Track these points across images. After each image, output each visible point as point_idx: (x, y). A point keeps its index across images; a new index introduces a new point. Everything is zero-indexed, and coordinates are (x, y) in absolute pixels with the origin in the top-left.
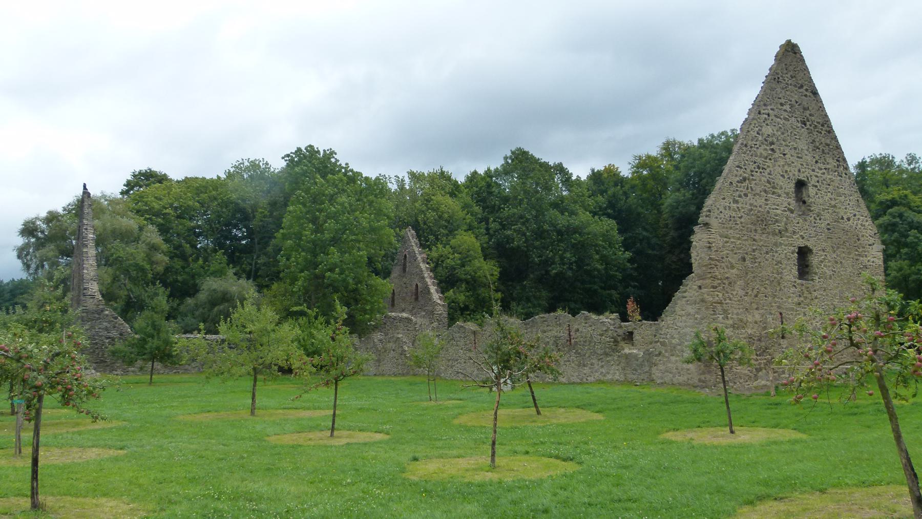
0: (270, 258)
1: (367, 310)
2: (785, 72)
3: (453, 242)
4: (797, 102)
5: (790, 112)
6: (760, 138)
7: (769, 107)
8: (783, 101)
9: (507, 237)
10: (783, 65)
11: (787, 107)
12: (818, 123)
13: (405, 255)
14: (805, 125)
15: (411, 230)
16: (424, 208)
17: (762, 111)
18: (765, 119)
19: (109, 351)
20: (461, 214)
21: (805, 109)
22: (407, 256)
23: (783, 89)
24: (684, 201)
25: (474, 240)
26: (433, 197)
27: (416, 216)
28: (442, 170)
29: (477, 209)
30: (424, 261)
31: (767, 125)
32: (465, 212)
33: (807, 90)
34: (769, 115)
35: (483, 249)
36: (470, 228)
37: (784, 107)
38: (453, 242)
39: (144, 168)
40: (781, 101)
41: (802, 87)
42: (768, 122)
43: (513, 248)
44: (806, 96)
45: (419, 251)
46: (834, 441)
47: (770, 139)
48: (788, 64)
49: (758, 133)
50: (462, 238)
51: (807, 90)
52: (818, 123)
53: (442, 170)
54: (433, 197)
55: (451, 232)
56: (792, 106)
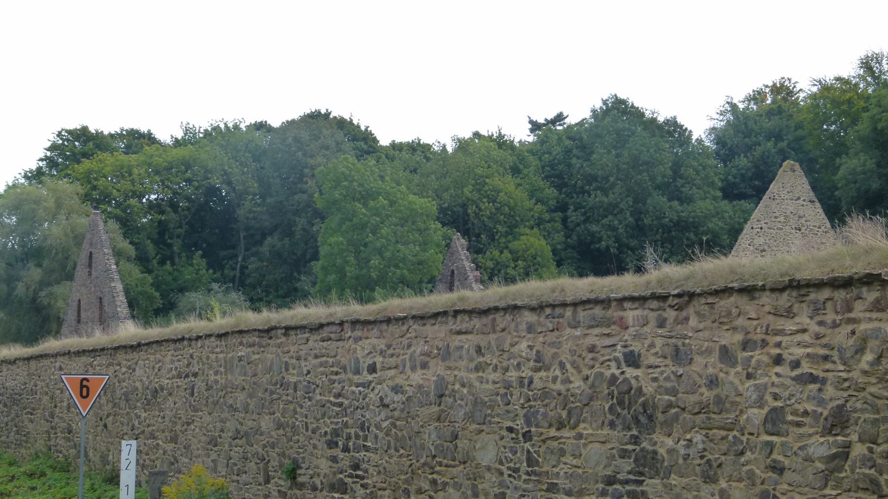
0: (262, 261)
1: (179, 206)
2: (782, 189)
3: (515, 245)
4: (792, 213)
5: (784, 222)
6: (752, 248)
7: (762, 222)
8: (777, 214)
9: (592, 235)
10: (780, 184)
11: (782, 219)
12: (814, 226)
13: (453, 272)
14: (800, 230)
15: (460, 237)
16: (476, 196)
17: (755, 227)
18: (758, 232)
19: (560, 414)
20: (528, 204)
21: (800, 217)
22: (456, 272)
23: (778, 204)
24: (864, 173)
25: (543, 242)
26: (487, 180)
27: (464, 206)
28: (500, 132)
29: (551, 192)
30: (476, 281)
31: (760, 236)
32: (533, 201)
33: (804, 200)
34: (761, 228)
35: (554, 252)
36: (539, 223)
37: (779, 219)
38: (515, 245)
39: (74, 124)
40: (775, 214)
41: (799, 198)
42: (761, 234)
43: (598, 250)
44: (803, 205)
45: (470, 267)
46: (322, 369)
47: (762, 248)
48: (786, 182)
49: (749, 245)
50: (528, 240)
51: (804, 200)
52: (814, 226)
53: (500, 132)
54: (487, 180)
55: (512, 230)
56: (786, 217)
